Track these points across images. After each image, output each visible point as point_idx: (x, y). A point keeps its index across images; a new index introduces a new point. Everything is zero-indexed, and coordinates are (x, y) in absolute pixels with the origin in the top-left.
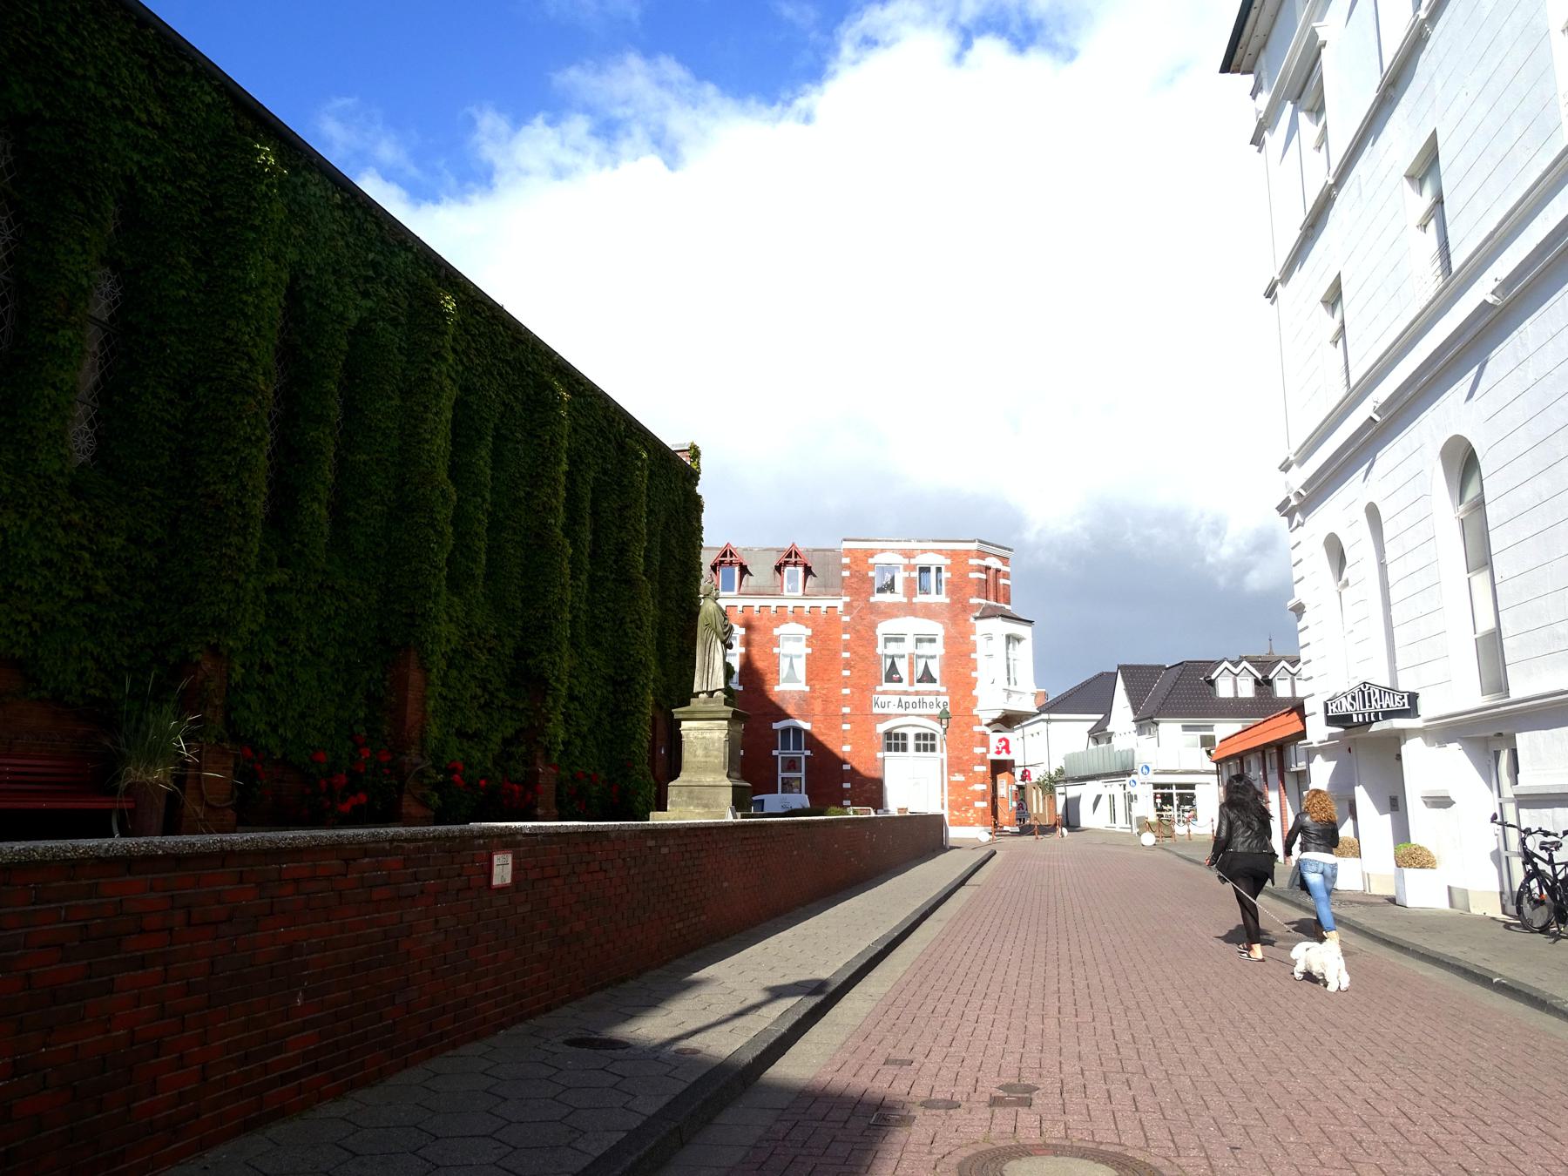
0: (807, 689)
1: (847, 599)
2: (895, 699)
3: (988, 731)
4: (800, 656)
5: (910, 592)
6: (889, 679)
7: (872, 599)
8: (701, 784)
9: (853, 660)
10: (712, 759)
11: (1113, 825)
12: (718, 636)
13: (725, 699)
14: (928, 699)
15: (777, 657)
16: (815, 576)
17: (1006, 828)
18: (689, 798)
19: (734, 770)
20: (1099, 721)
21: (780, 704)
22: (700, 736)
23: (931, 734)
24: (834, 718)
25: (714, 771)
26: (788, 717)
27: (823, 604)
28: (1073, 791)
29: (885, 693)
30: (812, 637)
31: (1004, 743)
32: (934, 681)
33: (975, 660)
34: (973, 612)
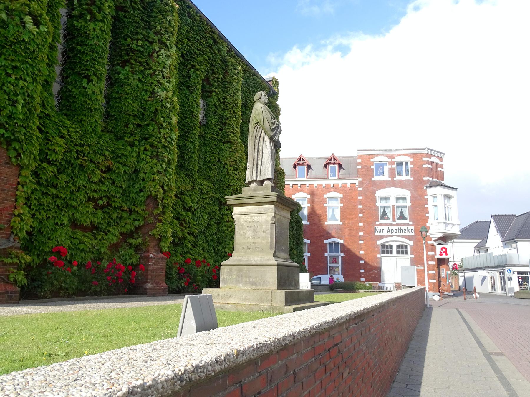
0: (341, 223)
1: (360, 179)
2: (386, 228)
3: (435, 244)
4: (338, 208)
5: (392, 175)
6: (382, 218)
7: (373, 179)
8: (249, 263)
9: (364, 209)
10: (260, 240)
11: (494, 292)
12: (265, 133)
13: (272, 186)
14: (403, 228)
15: (326, 208)
16: (344, 169)
17: (446, 293)
18: (238, 276)
19: (282, 251)
20: (480, 243)
21: (328, 231)
22: (249, 220)
23: (405, 245)
24: (355, 238)
25: (262, 251)
26: (332, 237)
27: (349, 182)
28: (468, 274)
29: (381, 225)
30: (343, 198)
31: (444, 250)
32: (406, 219)
33: (428, 208)
34: (425, 184)
